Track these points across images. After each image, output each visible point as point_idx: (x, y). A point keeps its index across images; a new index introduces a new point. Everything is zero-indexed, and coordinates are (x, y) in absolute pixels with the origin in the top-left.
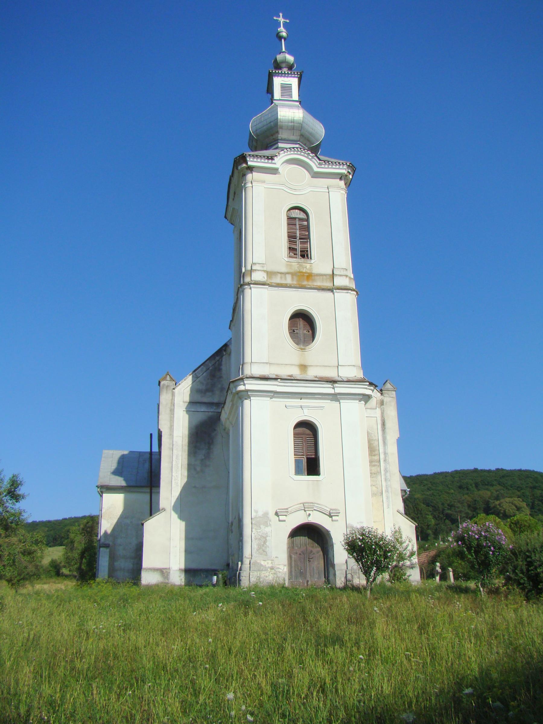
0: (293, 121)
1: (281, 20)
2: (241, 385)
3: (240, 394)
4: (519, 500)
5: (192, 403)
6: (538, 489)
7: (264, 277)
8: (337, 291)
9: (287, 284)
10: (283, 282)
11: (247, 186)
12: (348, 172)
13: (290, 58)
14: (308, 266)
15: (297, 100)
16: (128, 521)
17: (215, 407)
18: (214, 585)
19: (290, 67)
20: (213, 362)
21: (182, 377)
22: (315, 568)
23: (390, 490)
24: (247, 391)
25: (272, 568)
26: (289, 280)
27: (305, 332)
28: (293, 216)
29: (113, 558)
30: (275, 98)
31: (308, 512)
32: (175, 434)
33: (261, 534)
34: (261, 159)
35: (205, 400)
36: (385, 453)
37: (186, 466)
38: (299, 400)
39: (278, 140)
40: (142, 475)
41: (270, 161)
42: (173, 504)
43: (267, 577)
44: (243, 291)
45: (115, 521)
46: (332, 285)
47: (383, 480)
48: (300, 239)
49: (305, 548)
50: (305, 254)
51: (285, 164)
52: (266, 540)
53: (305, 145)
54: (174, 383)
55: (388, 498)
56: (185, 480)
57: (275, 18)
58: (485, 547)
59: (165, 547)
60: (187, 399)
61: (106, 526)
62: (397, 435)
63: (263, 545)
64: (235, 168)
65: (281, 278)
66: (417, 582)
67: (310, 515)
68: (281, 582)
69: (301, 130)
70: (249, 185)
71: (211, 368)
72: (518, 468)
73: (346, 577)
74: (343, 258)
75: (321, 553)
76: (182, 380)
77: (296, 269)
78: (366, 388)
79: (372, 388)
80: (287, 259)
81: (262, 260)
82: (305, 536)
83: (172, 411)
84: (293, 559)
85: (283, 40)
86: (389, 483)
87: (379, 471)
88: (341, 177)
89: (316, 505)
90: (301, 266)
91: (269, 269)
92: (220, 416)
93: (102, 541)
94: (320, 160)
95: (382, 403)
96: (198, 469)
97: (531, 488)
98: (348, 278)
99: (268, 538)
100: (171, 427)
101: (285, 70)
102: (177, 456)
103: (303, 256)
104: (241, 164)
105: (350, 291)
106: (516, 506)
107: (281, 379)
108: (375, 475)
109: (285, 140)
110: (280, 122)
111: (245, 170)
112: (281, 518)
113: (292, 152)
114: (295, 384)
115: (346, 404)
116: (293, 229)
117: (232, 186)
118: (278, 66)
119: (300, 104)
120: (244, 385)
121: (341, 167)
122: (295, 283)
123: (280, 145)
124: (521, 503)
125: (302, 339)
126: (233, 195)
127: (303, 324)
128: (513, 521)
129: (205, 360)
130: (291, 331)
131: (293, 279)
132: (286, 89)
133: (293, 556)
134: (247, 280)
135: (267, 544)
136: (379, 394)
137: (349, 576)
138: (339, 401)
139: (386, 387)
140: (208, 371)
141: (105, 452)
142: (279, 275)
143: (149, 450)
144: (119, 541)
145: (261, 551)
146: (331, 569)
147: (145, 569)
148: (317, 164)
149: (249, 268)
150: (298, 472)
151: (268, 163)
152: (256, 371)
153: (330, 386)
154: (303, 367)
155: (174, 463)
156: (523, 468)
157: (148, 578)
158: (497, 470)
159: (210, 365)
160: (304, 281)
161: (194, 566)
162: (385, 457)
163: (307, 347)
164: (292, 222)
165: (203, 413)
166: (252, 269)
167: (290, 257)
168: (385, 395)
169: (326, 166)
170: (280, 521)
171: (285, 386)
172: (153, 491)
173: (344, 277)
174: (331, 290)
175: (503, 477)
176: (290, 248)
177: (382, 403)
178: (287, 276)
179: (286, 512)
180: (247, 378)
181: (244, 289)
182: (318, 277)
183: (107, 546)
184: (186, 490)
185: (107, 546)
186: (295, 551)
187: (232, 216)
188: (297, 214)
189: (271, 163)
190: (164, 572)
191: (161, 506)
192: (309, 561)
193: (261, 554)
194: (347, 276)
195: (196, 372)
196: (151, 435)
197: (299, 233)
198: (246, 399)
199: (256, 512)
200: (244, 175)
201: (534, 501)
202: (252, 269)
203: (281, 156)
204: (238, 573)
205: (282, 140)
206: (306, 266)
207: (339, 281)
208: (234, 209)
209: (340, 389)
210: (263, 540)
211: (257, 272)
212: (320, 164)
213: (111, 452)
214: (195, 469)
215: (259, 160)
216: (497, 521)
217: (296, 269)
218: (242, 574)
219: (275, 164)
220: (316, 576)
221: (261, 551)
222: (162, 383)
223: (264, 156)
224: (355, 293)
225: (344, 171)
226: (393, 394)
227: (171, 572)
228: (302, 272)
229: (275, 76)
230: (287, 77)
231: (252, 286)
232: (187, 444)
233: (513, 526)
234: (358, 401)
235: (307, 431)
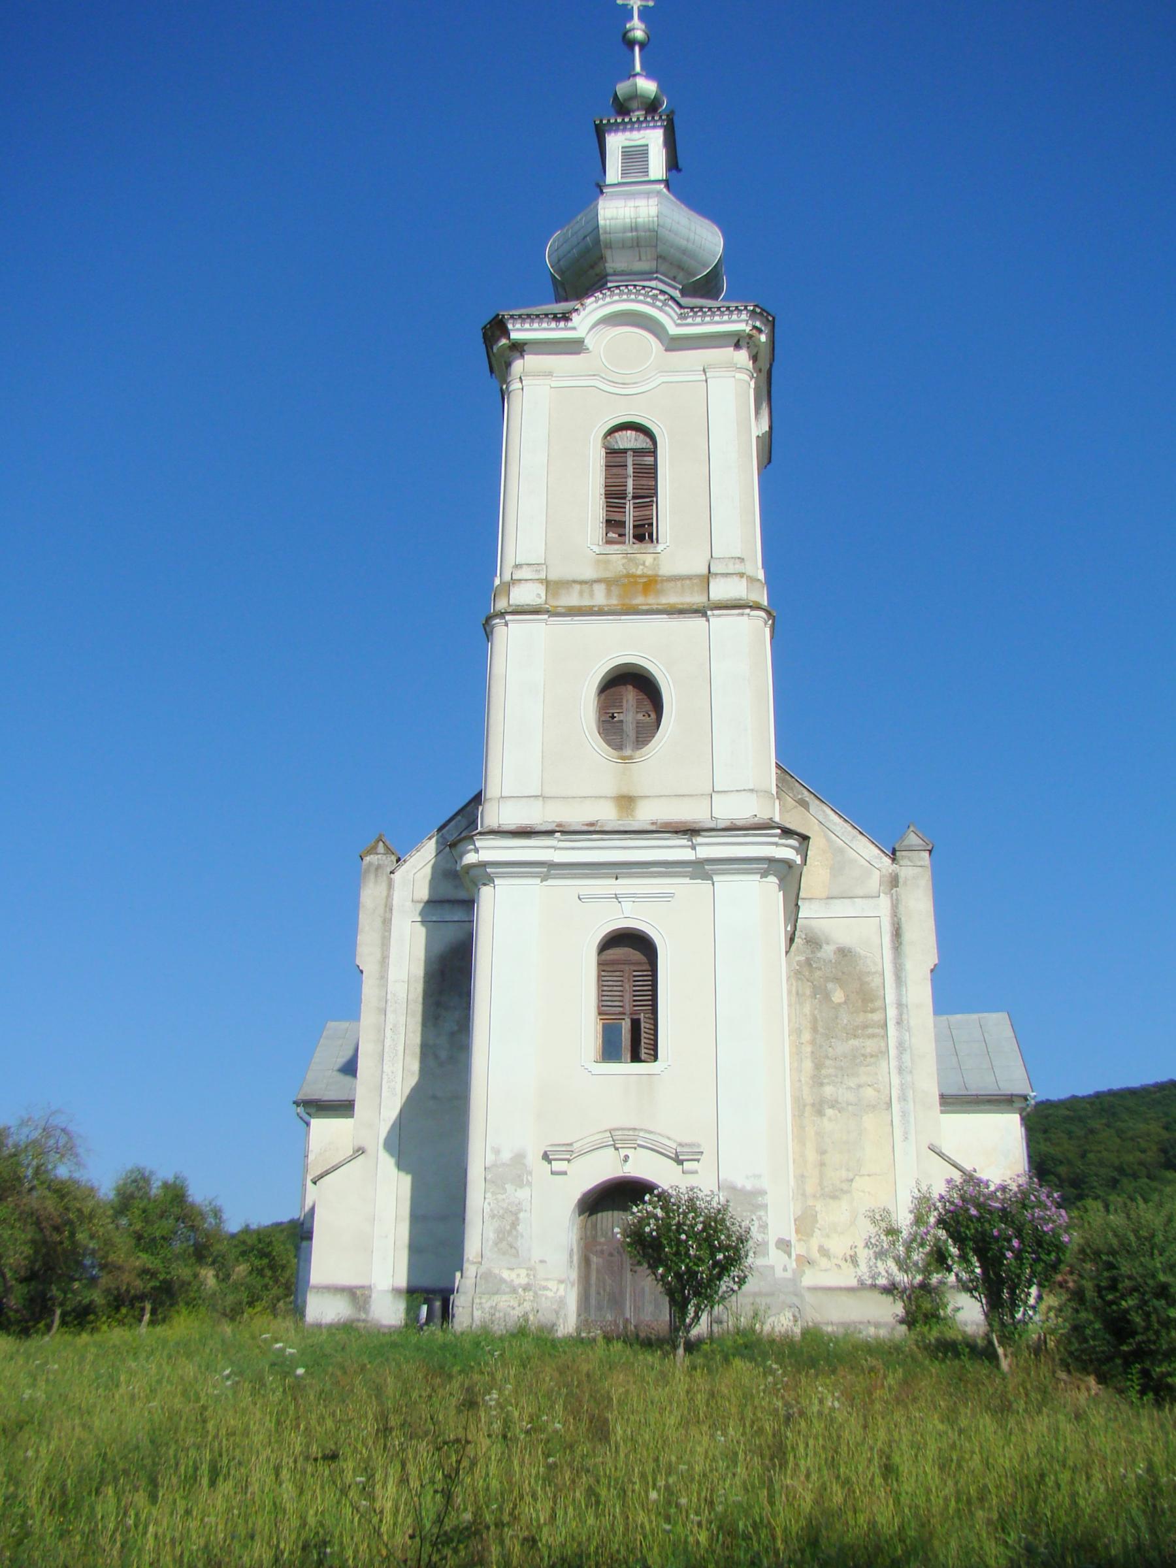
0: (634, 228)
3: (473, 872)
7: (539, 596)
8: (716, 612)
10: (586, 602)
11: (511, 388)
13: (647, 86)
14: (649, 559)
21: (413, 844)
23: (910, 1094)
24: (483, 865)
26: (600, 597)
27: (640, 717)
30: (608, 182)
31: (623, 1152)
33: (505, 1205)
34: (541, 321)
36: (900, 1005)
38: (613, 881)
39: (607, 275)
41: (562, 324)
47: (894, 1072)
48: (634, 498)
50: (644, 533)
51: (601, 326)
52: (518, 1219)
53: (674, 279)
54: (394, 858)
55: (904, 1114)
56: (413, 1080)
58: (996, 1239)
60: (424, 893)
62: (931, 958)
63: (510, 1232)
65: (581, 593)
66: (978, 1325)
67: (626, 1158)
68: (546, 1317)
69: (656, 246)
76: (411, 850)
78: (776, 844)
81: (537, 556)
83: (387, 922)
84: (594, 1267)
85: (637, 49)
86: (909, 1078)
87: (884, 1049)
89: (641, 1134)
90: (631, 560)
91: (553, 576)
94: (681, 306)
95: (894, 881)
96: (443, 1055)
98: (744, 580)
99: (521, 1215)
100: (384, 961)
101: (639, 114)
103: (639, 538)
104: (498, 340)
105: (747, 611)
107: (563, 832)
108: (872, 1060)
109: (622, 273)
110: (605, 233)
111: (507, 352)
113: (616, 298)
115: (728, 886)
119: (668, 187)
120: (477, 850)
121: (734, 317)
122: (614, 601)
127: (631, 697)
129: (467, 801)
130: (606, 717)
131: (609, 593)
132: (635, 157)
135: (519, 1228)
136: (887, 861)
138: (712, 879)
139: (906, 843)
142: (577, 587)
145: (504, 1245)
147: (314, 1287)
148: (676, 317)
153: (685, 842)
154: (626, 802)
155: (388, 1042)
157: (322, 1310)
160: (635, 596)
162: (901, 1014)
163: (638, 753)
164: (618, 459)
167: (609, 542)
168: (902, 863)
169: (699, 320)
170: (552, 1173)
171: (573, 848)
173: (736, 579)
174: (701, 612)
176: (608, 522)
177: (894, 881)
178: (596, 587)
179: (569, 1153)
182: (672, 584)
186: (599, 1248)
188: (628, 440)
189: (566, 329)
190: (357, 1295)
193: (504, 1254)
194: (741, 575)
195: (444, 831)
197: (631, 487)
198: (485, 884)
199: (497, 1152)
203: (588, 309)
205: (615, 274)
206: (645, 559)
207: (720, 590)
209: (708, 848)
211: (524, 586)
214: (436, 1057)
219: (574, 329)
223: (546, 315)
226: (923, 859)
227: (374, 1296)
229: (610, 131)
230: (639, 129)
231: (508, 617)
232: (420, 999)
235: (630, 955)
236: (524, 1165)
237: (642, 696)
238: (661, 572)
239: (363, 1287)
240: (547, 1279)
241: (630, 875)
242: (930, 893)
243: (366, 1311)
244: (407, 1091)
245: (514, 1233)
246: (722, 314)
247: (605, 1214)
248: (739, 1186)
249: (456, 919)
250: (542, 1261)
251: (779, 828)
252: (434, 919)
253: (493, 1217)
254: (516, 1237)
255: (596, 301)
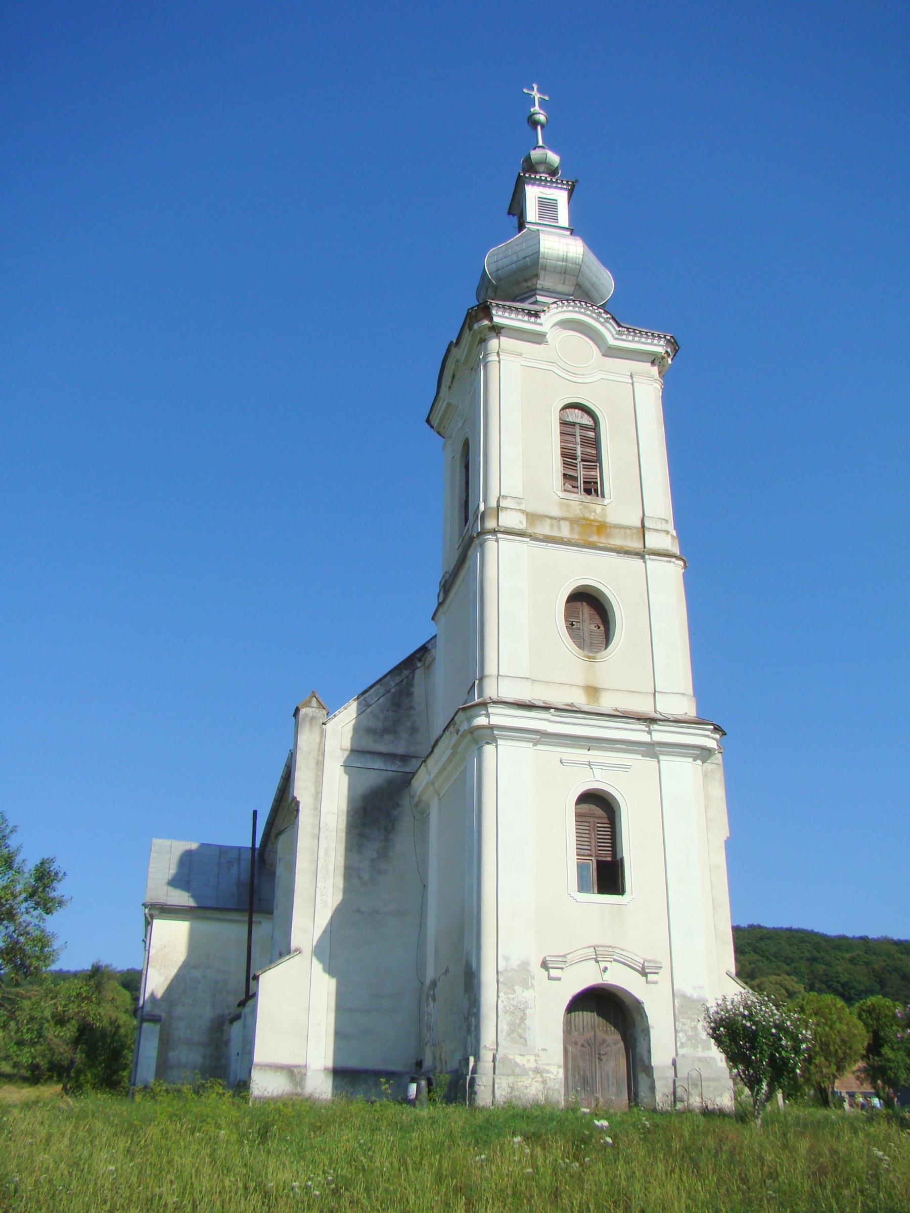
0: (565, 260)
1: (536, 95)
2: (481, 715)
3: (476, 733)
4: (792, 980)
5: (357, 752)
6: (820, 963)
7: (521, 522)
9: (562, 538)
10: (555, 533)
11: (490, 359)
12: (667, 352)
13: (554, 158)
14: (599, 509)
15: (567, 226)
16: (197, 974)
17: (399, 763)
18: (412, 1103)
19: (553, 172)
20: (398, 679)
22: (610, 1074)
24: (492, 728)
25: (537, 1071)
26: (565, 531)
27: (592, 627)
28: (571, 419)
29: (165, 1044)
31: (603, 965)
32: (324, 808)
33: (515, 1003)
35: (382, 748)
37: (341, 870)
38: (585, 752)
39: (536, 289)
40: (243, 889)
41: (533, 319)
42: (315, 943)
43: (526, 1087)
44: (482, 545)
45: (173, 972)
46: (642, 546)
49: (592, 1034)
50: (592, 488)
51: (557, 327)
52: (525, 1014)
54: (325, 712)
56: (339, 897)
57: (525, 91)
59: (297, 1025)
60: (347, 744)
61: (156, 983)
63: (519, 1025)
64: (467, 326)
65: (552, 526)
67: (606, 969)
70: (493, 358)
71: (393, 690)
72: (786, 925)
73: (674, 1093)
74: (659, 503)
75: (621, 1044)
77: (578, 512)
78: (708, 736)
79: (717, 736)
80: (562, 494)
81: (518, 492)
82: (592, 1011)
83: (320, 764)
84: (570, 1055)
85: (539, 128)
88: (655, 359)
89: (617, 951)
90: (585, 507)
91: (530, 509)
92: (411, 779)
93: (147, 1008)
94: (619, 326)
96: (366, 876)
97: (808, 960)
98: (669, 536)
99: (528, 1012)
100: (318, 795)
102: (326, 850)
103: (588, 491)
104: (478, 321)
105: (674, 560)
106: (787, 990)
107: (557, 709)
109: (547, 290)
112: (554, 973)
113: (571, 308)
114: (580, 719)
116: (569, 442)
117: (450, 363)
118: (530, 166)
120: (488, 715)
121: (655, 342)
122: (576, 536)
123: (539, 298)
124: (796, 986)
125: (587, 639)
126: (450, 379)
127: (590, 610)
128: (864, 1007)
131: (572, 529)
132: (548, 207)
133: (570, 1049)
134: (490, 524)
135: (527, 1022)
137: (679, 1091)
138: (658, 758)
140: (389, 695)
141: (156, 841)
142: (548, 521)
143: (251, 846)
144: (179, 1010)
145: (515, 1035)
146: (642, 1078)
147: (258, 1065)
148: (614, 333)
149: (493, 503)
150: (583, 887)
151: (528, 322)
152: (509, 691)
153: (643, 727)
154: (593, 691)
156: (795, 926)
157: (265, 1084)
158: (751, 927)
159: (393, 684)
160: (592, 535)
161: (353, 1063)
163: (599, 655)
164: (570, 430)
165: (377, 773)
166: (498, 506)
167: (565, 491)
169: (630, 338)
170: (550, 978)
171: (561, 723)
172: (254, 919)
173: (664, 534)
174: (641, 555)
175: (761, 939)
176: (565, 475)
178: (562, 523)
179: (563, 961)
180: (494, 702)
181: (485, 540)
182: (617, 531)
183: (155, 1019)
184: (339, 912)
185: (155, 1019)
186: (573, 1040)
187: (442, 419)
189: (535, 323)
190: (295, 1073)
191: (294, 944)
192: (600, 1059)
193: (516, 1042)
194: (667, 532)
196: (255, 813)
197: (582, 452)
198: (488, 743)
199: (507, 959)
200: (483, 341)
201: (813, 983)
202: (498, 506)
203: (552, 312)
204: (468, 1078)
205: (542, 290)
206: (596, 509)
207: (654, 541)
208: (449, 404)
209: (661, 734)
210: (520, 1014)
211: (509, 512)
212: (619, 333)
213: (167, 842)
214: (360, 878)
215: (513, 316)
216: (839, 1006)
217: (578, 512)
218: (478, 1081)
219: (541, 324)
220: (613, 1089)
221: (515, 1035)
222: (303, 711)
223: (523, 310)
224: (682, 563)
225: (661, 350)
227: (309, 1074)
228: (587, 519)
229: (528, 184)
230: (550, 187)
231: (499, 535)
233: (864, 1015)
234: (691, 759)
235: (599, 808)
236: (528, 970)
237: (593, 612)
238: (607, 520)
239: (299, 1066)
240: (549, 1064)
241: (599, 749)
242: (723, 785)
243: (303, 1088)
244: (335, 906)
245: (523, 1026)
246: (635, 336)
247: (577, 1013)
248: (689, 994)
249: (376, 767)
250: (543, 1050)
251: (712, 725)
252: (359, 765)
253: (506, 1012)
254: (525, 1029)
255: (557, 308)
